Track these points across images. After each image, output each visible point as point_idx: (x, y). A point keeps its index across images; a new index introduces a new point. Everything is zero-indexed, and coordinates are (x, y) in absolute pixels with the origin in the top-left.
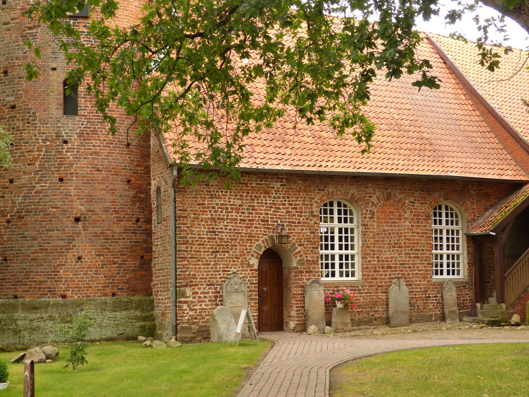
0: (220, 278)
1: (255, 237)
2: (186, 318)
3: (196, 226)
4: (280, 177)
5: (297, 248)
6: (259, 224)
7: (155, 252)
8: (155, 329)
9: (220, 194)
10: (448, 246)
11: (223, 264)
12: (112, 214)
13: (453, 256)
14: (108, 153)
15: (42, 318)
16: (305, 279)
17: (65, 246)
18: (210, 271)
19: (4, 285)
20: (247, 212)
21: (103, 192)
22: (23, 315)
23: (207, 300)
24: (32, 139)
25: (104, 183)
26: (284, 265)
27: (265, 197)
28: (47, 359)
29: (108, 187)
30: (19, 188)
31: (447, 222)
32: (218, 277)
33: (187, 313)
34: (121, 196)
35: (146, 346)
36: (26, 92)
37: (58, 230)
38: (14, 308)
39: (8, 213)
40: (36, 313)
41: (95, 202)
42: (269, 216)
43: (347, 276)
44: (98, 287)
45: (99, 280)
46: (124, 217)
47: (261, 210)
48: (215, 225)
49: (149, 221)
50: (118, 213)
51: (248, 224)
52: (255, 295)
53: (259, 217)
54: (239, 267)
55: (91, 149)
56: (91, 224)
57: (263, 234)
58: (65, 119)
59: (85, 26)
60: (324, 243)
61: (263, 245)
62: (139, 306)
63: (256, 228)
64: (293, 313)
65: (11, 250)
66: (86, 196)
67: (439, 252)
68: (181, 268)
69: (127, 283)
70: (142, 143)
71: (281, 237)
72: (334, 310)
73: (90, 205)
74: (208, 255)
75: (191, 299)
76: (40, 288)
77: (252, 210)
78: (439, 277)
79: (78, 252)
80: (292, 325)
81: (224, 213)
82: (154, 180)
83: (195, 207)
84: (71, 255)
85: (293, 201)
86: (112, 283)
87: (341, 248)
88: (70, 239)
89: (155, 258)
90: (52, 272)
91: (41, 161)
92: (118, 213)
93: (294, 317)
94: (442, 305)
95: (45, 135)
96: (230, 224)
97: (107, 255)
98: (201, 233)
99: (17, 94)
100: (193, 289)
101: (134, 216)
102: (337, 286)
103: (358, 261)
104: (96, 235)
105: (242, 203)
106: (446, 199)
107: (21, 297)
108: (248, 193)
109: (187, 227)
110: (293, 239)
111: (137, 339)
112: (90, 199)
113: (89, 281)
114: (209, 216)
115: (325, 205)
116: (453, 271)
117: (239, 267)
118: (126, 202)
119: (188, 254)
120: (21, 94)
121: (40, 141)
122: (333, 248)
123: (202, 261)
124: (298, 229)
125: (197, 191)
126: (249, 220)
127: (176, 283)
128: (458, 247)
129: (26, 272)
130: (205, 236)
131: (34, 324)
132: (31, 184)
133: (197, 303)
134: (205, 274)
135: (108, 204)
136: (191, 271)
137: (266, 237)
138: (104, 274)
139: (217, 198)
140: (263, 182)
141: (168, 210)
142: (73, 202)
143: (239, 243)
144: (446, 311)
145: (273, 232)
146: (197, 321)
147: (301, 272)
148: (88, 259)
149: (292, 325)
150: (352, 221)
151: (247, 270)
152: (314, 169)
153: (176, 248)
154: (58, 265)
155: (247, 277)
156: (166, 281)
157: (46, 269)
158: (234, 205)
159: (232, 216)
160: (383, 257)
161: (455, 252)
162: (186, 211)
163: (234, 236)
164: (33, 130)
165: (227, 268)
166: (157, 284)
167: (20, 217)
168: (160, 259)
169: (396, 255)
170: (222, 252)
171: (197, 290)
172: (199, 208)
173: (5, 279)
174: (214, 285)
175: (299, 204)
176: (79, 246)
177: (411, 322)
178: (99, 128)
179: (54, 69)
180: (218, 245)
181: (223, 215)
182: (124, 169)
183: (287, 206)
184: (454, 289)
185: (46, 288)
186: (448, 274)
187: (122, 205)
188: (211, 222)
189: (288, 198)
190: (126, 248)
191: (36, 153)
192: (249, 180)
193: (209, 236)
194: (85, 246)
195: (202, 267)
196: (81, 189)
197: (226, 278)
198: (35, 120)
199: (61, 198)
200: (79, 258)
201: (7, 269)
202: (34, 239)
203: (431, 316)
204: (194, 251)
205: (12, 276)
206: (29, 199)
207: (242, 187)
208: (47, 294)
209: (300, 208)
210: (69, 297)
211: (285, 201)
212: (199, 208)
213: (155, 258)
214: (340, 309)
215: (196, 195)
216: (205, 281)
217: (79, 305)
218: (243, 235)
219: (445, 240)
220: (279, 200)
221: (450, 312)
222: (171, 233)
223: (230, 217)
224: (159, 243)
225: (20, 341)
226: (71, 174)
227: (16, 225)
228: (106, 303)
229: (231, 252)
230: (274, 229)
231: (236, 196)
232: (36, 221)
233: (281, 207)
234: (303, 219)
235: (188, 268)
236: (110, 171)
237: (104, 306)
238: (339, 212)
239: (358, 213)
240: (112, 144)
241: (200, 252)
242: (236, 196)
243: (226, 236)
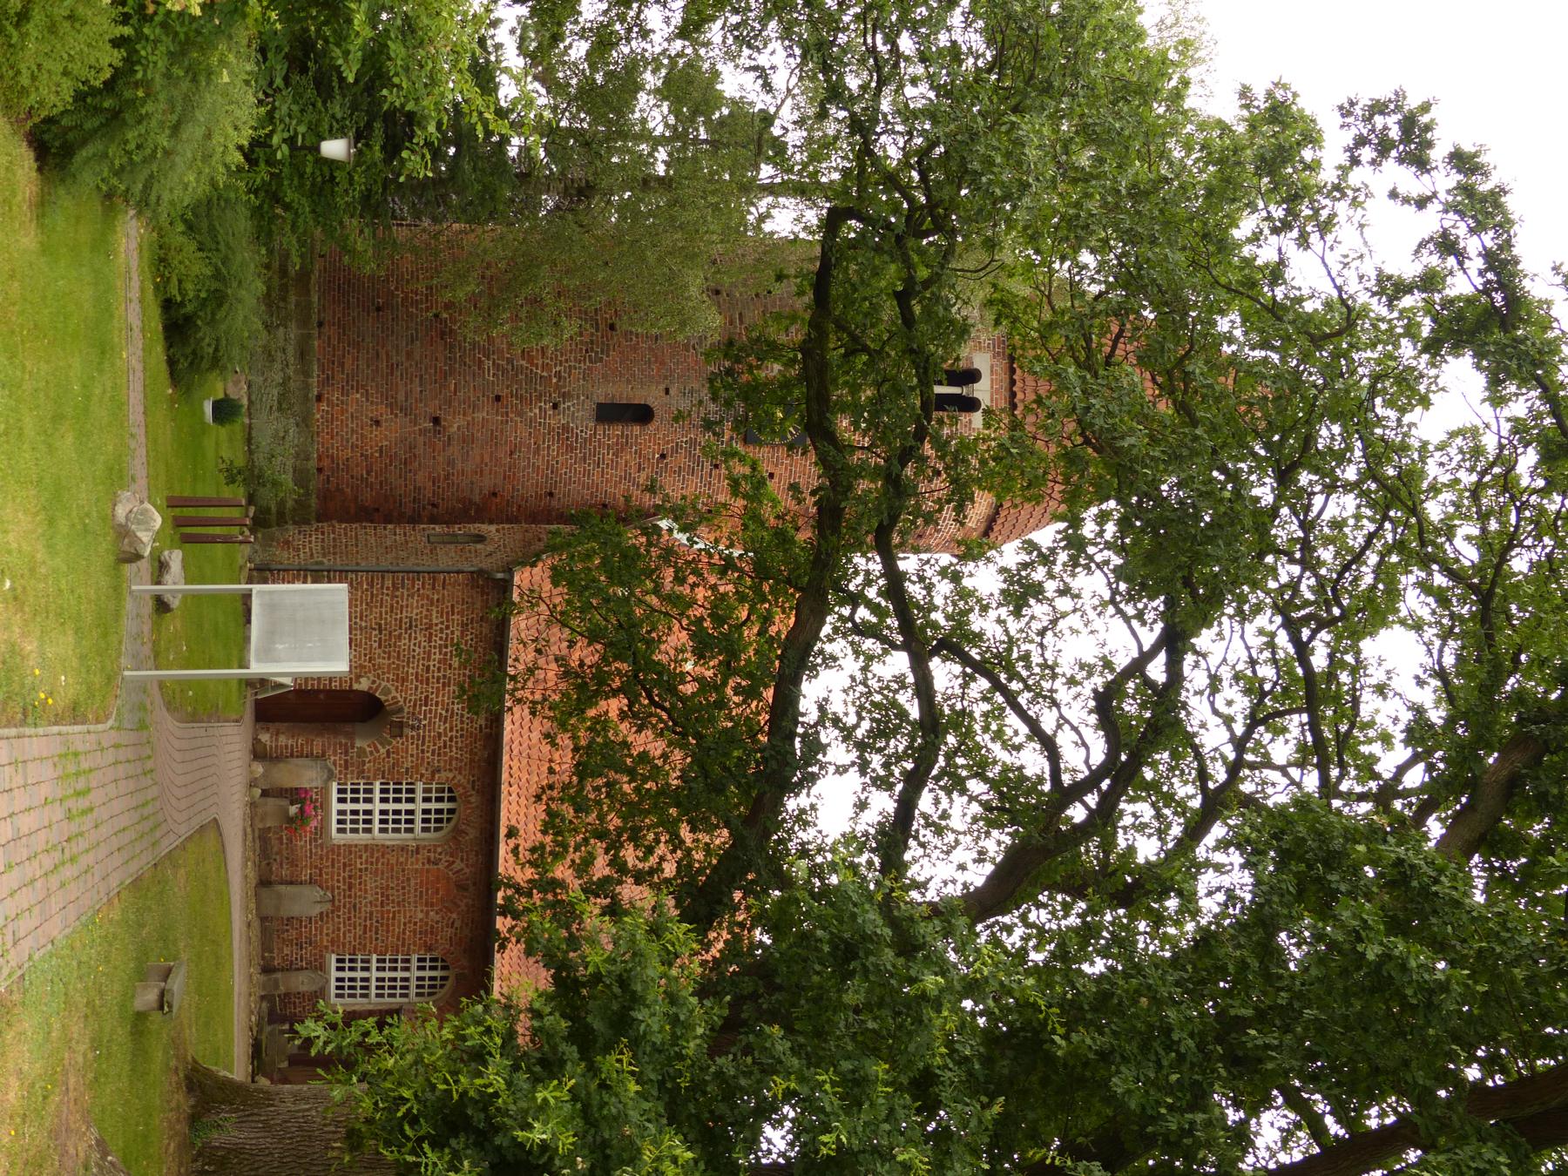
10: (383, 980)
13: (367, 988)
16: (334, 758)
21: (478, 459)
26: (359, 726)
31: (422, 979)
36: (635, 349)
38: (304, 322)
43: (339, 822)
49: (433, 520)
58: (590, 406)
60: (391, 787)
62: (301, 504)
64: (283, 740)
67: (374, 965)
69: (338, 489)
71: (401, 725)
72: (285, 802)
78: (334, 965)
80: (265, 738)
84: (381, 410)
87: (382, 812)
94: (289, 968)
102: (324, 806)
103: (362, 838)
106: (458, 977)
110: (397, 742)
112: (467, 441)
115: (450, 790)
116: (342, 988)
122: (383, 800)
128: (382, 996)
141: (447, 558)
144: (279, 975)
147: (346, 753)
149: (265, 738)
150: (424, 830)
152: (505, 776)
160: (367, 878)
161: (373, 991)
167: (442, 335)
169: (370, 898)
177: (263, 919)
179: (667, 391)
184: (313, 988)
186: (338, 980)
200: (378, 423)
202: (409, 355)
203: (271, 951)
214: (287, 811)
217: (305, 421)
219: (393, 974)
221: (276, 981)
222: (410, 564)
238: (438, 811)
239: (436, 839)
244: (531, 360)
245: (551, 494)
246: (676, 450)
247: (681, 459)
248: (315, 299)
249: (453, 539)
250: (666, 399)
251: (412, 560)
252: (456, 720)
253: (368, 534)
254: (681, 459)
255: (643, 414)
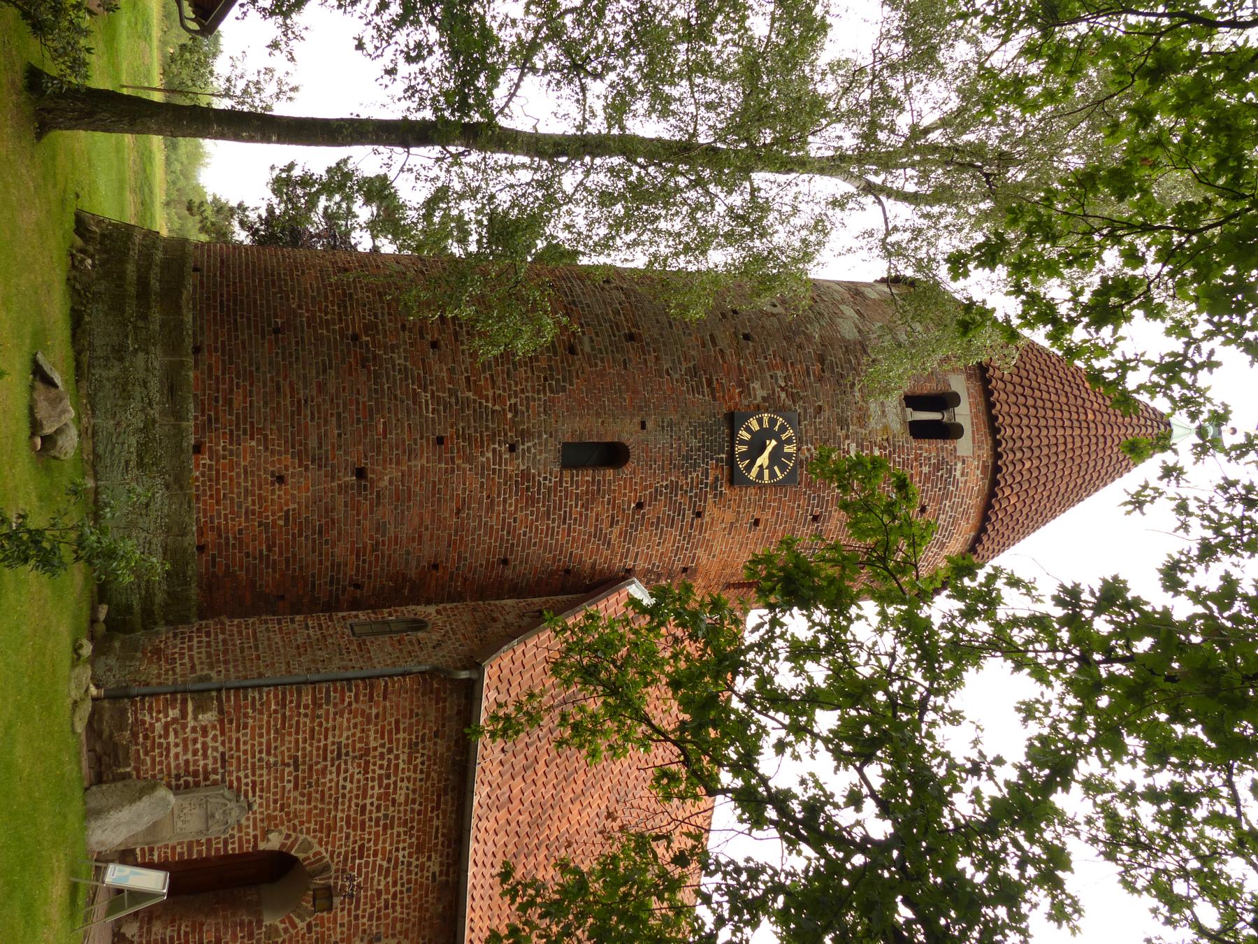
0: (239, 779)
1: (328, 836)
2: (147, 718)
3: (353, 721)
4: (451, 870)
5: (303, 920)
6: (355, 842)
7: (293, 621)
8: (125, 632)
9: (419, 761)
11: (269, 781)
12: (371, 538)
14: (492, 527)
15: (150, 404)
17: (306, 450)
18: (253, 756)
19: (222, 327)
20: (380, 815)
21: (416, 521)
22: (156, 364)
23: (189, 756)
24: (516, 385)
25: (433, 521)
27: (411, 845)
28: (44, 439)
29: (427, 529)
30: (423, 360)
32: (242, 774)
33: (157, 719)
34: (408, 553)
35: (76, 649)
36: (602, 374)
37: (340, 435)
38: (174, 347)
39: (373, 337)
40: (161, 391)
41: (396, 508)
42: (371, 859)
44: (219, 517)
45: (233, 520)
46: (364, 561)
47: (385, 841)
48: (354, 758)
49: (355, 605)
50: (373, 551)
51: (355, 820)
52: (200, 852)
53: (369, 840)
54: (261, 813)
55: (499, 496)
56: (353, 499)
57: (333, 852)
58: (554, 446)
59: (716, 479)
61: (311, 854)
63: (347, 837)
65: (297, 343)
66: (409, 488)
68: (261, 698)
70: (506, 586)
73: (391, 498)
74: (289, 750)
75: (191, 723)
76: (217, 400)
77: (385, 825)
79: (293, 476)
81: (378, 772)
82: (438, 612)
83: (392, 715)
85: (402, 899)
86: (227, 544)
88: (320, 459)
89: (279, 622)
90: (252, 424)
91: (475, 401)
92: (373, 551)
93: (149, 931)
95: (524, 409)
96: (355, 785)
97: (287, 533)
98: (337, 732)
99: (595, 357)
100: (214, 727)
101: (366, 580)
104: (329, 510)
105: (400, 805)
107: (196, 362)
108: (419, 813)
109: (350, 704)
111: (101, 602)
113: (232, 499)
114: (373, 744)
117: (261, 813)
118: (395, 563)
119: (291, 709)
120: (596, 365)
121: (513, 401)
123: (276, 739)
124: (343, 917)
125: (425, 715)
126: (363, 823)
127: (228, 689)
129: (251, 372)
130: (330, 739)
131: (138, 388)
132: (431, 384)
133: (181, 736)
134: (249, 747)
135: (392, 530)
136: (254, 718)
137: (328, 859)
138: (247, 527)
139: (410, 755)
140: (441, 839)
142: (398, 463)
143: (316, 807)
145: (337, 871)
146: (141, 740)
148: (279, 497)
151: (255, 829)
153: (305, 683)
154: (266, 436)
155: (240, 830)
156: (230, 657)
157: (259, 411)
158: (395, 788)
159: (373, 788)
162: (385, 698)
163: (330, 796)
164: (533, 387)
165: (262, 790)
166: (223, 633)
168: (277, 638)
170: (296, 778)
171: (211, 734)
172: (390, 724)
173: (236, 330)
174: (223, 767)
175: (394, 911)
176: (306, 478)
178: (538, 508)
179: (643, 425)
180: (311, 768)
181: (374, 771)
182: (459, 557)
183: (392, 891)
185: (217, 413)
187: (390, 557)
188: (360, 749)
189: (409, 890)
190: (301, 568)
191: (490, 394)
192: (444, 812)
193: (330, 748)
194: (307, 490)
195: (264, 740)
196: (422, 479)
197: (239, 789)
198: (552, 391)
199: (404, 441)
200: (281, 479)
201: (256, 333)
202: (321, 388)
204: (298, 722)
205: (243, 343)
206: (401, 380)
207: (432, 801)
208: (203, 415)
209: (387, 916)
210: (197, 460)
211: (403, 885)
212: (390, 724)
213: (279, 622)
215: (417, 715)
216: (231, 749)
217: (178, 481)
218: (333, 813)
220: (404, 874)
222: (333, 670)
223: (370, 784)
224: (311, 631)
225: (98, 358)
226: (453, 459)
227: (349, 352)
228: (183, 535)
229: (297, 794)
230: (344, 871)
231: (414, 791)
232: (358, 393)
233: (390, 879)
234: (364, 924)
235: (261, 713)
236: (456, 532)
237: (175, 530)
240: (508, 533)
241: (297, 733)
242: (414, 791)
243: (331, 781)
244: (478, 391)
245: (505, 562)
246: (654, 498)
247: (661, 508)
248: (188, 318)
249: (386, 628)
250: (642, 435)
251: (337, 661)
252: (401, 872)
253: (270, 633)
254: (661, 508)
255: (614, 455)
